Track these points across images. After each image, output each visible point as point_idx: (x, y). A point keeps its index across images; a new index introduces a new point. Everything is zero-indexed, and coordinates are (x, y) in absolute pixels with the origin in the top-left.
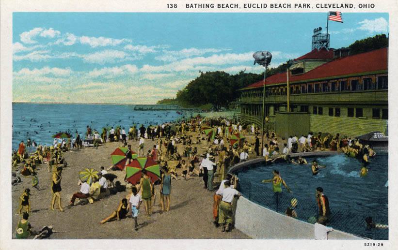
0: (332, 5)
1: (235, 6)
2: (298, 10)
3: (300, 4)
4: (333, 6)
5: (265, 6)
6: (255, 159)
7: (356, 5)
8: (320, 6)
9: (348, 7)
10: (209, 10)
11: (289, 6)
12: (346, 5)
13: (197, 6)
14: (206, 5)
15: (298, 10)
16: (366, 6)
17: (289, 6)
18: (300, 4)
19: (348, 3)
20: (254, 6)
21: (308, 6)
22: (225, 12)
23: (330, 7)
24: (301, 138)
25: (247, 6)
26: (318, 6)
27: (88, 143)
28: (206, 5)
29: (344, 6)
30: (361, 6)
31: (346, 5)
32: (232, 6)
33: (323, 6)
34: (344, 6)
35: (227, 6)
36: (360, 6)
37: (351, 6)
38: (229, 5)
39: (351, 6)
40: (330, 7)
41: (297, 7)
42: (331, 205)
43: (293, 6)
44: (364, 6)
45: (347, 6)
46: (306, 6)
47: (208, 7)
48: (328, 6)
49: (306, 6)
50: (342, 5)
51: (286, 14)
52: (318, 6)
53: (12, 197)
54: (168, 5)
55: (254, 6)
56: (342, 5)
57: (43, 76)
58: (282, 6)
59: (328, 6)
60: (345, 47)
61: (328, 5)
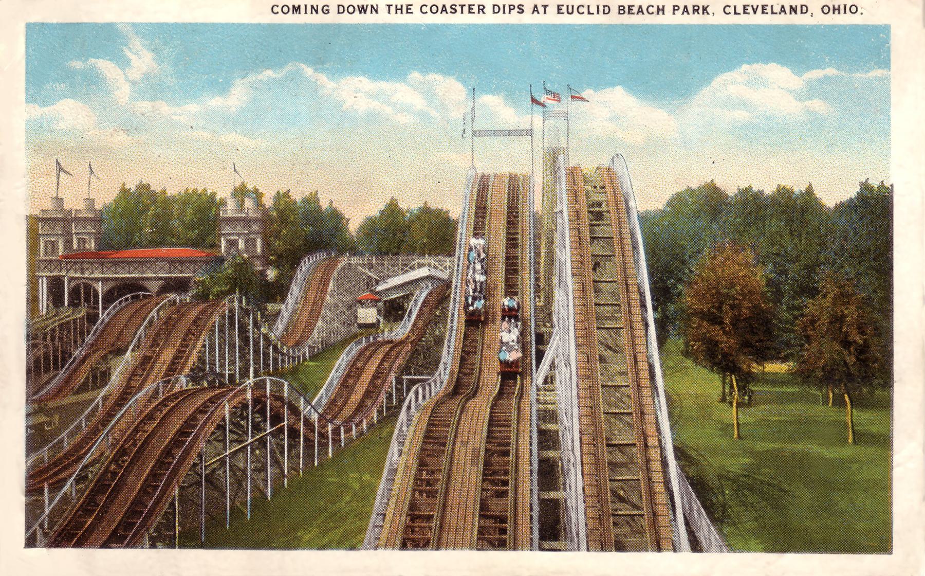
0: (760, 9)
1: (658, 10)
2: (680, 19)
4: (629, 10)
6: (335, 368)
7: (815, 8)
12: (791, 7)
14: (312, 7)
15: (680, 19)
16: (401, 9)
17: (481, 9)
18: (686, 7)
20: (651, 10)
22: (654, 22)
23: (755, 13)
26: (727, 10)
28: (312, 7)
32: (651, 10)
33: (740, 9)
35: (444, 9)
36: (496, 9)
37: (804, 9)
39: (804, 9)
40: (755, 13)
41: (514, 12)
42: (856, 428)
43: (669, 9)
46: (701, 11)
47: (317, 12)
48: (750, 10)
49: (701, 11)
50: (783, 7)
51: (475, 26)
52: (727, 10)
54: (545, 13)
55: (581, 10)
56: (783, 7)
57: (549, 416)
58: (645, 11)
59: (750, 10)
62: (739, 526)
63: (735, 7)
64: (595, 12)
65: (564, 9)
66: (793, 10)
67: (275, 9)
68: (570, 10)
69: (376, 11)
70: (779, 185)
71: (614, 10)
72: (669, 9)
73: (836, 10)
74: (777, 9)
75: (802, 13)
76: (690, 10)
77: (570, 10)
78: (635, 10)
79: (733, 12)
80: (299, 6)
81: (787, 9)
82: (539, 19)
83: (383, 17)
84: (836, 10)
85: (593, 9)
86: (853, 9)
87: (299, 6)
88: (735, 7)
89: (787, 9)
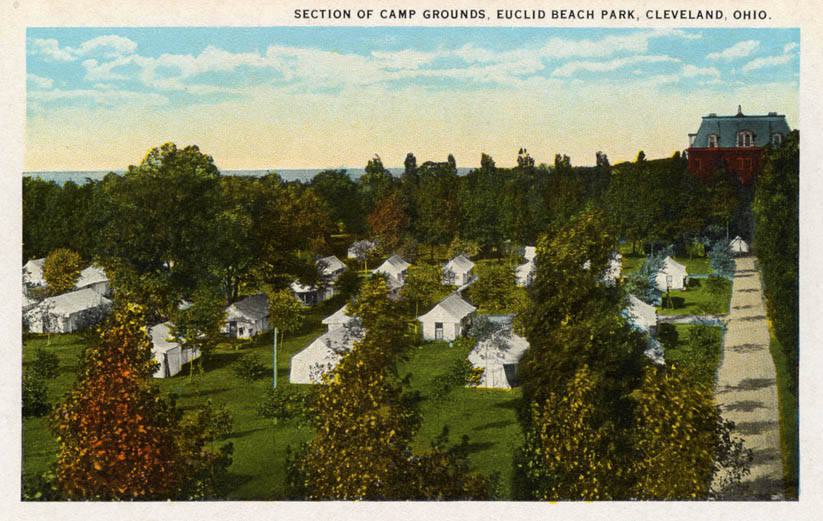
1: (588, 14)
3: (613, 12)
5: (541, 15)
7: (491, 13)
8: (522, 14)
9: (466, 16)
10: (343, 22)
11: (591, 15)
12: (708, 12)
13: (326, 14)
14: (462, 12)
15: (327, 22)
16: (749, 15)
17: (591, 15)
18: (613, 12)
19: (713, 9)
20: (581, 14)
21: (630, 14)
23: (675, 17)
24: (307, 381)
25: (504, 14)
26: (650, 14)
27: (490, 226)
29: (704, 16)
30: (737, 15)
31: (708, 12)
32: (581, 14)
33: (661, 14)
34: (704, 16)
35: (572, 14)
37: (719, 15)
38: (576, 14)
39: (719, 15)
40: (675, 17)
41: (607, 17)
43: (598, 14)
44: (745, 15)
45: (709, 15)
46: (626, 15)
47: (345, 12)
49: (626, 15)
50: (700, 12)
52: (384, 14)
53: (24, 364)
56: (700, 12)
58: (576, 15)
60: (122, 168)
61: (670, 13)
62: (178, 405)
63: (657, 12)
64: (531, 16)
65: (504, 14)
66: (709, 15)
67: (650, 14)
68: (454, 15)
69: (349, 16)
70: (558, 156)
71: (549, 15)
72: (598, 14)
73: (747, 15)
74: (695, 14)
75: (717, 17)
76: (617, 15)
77: (454, 15)
78: (567, 14)
79: (655, 17)
80: (405, 12)
81: (704, 14)
82: (366, 23)
83: (418, 20)
84: (747, 15)
85: (530, 14)
86: (763, 15)
87: (405, 12)
88: (657, 12)
89: (704, 14)
